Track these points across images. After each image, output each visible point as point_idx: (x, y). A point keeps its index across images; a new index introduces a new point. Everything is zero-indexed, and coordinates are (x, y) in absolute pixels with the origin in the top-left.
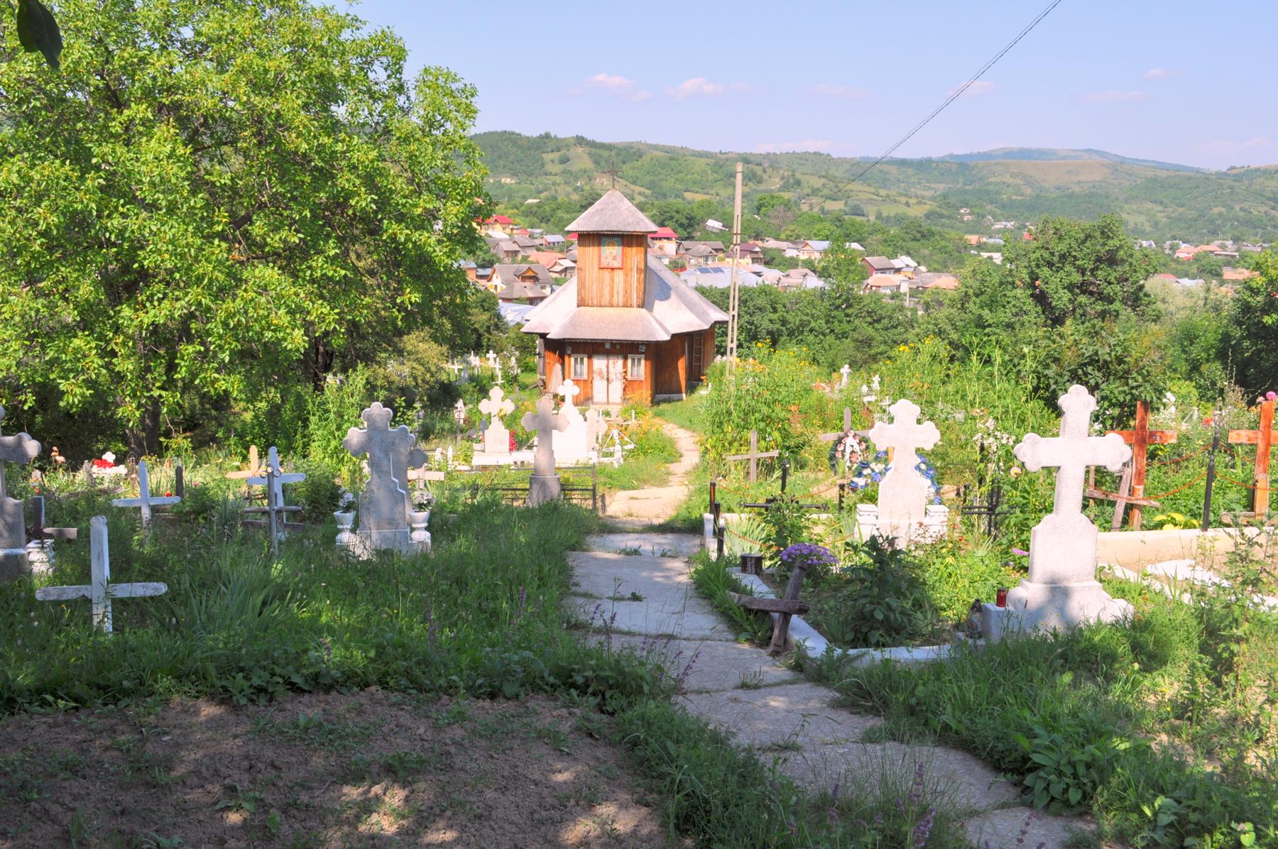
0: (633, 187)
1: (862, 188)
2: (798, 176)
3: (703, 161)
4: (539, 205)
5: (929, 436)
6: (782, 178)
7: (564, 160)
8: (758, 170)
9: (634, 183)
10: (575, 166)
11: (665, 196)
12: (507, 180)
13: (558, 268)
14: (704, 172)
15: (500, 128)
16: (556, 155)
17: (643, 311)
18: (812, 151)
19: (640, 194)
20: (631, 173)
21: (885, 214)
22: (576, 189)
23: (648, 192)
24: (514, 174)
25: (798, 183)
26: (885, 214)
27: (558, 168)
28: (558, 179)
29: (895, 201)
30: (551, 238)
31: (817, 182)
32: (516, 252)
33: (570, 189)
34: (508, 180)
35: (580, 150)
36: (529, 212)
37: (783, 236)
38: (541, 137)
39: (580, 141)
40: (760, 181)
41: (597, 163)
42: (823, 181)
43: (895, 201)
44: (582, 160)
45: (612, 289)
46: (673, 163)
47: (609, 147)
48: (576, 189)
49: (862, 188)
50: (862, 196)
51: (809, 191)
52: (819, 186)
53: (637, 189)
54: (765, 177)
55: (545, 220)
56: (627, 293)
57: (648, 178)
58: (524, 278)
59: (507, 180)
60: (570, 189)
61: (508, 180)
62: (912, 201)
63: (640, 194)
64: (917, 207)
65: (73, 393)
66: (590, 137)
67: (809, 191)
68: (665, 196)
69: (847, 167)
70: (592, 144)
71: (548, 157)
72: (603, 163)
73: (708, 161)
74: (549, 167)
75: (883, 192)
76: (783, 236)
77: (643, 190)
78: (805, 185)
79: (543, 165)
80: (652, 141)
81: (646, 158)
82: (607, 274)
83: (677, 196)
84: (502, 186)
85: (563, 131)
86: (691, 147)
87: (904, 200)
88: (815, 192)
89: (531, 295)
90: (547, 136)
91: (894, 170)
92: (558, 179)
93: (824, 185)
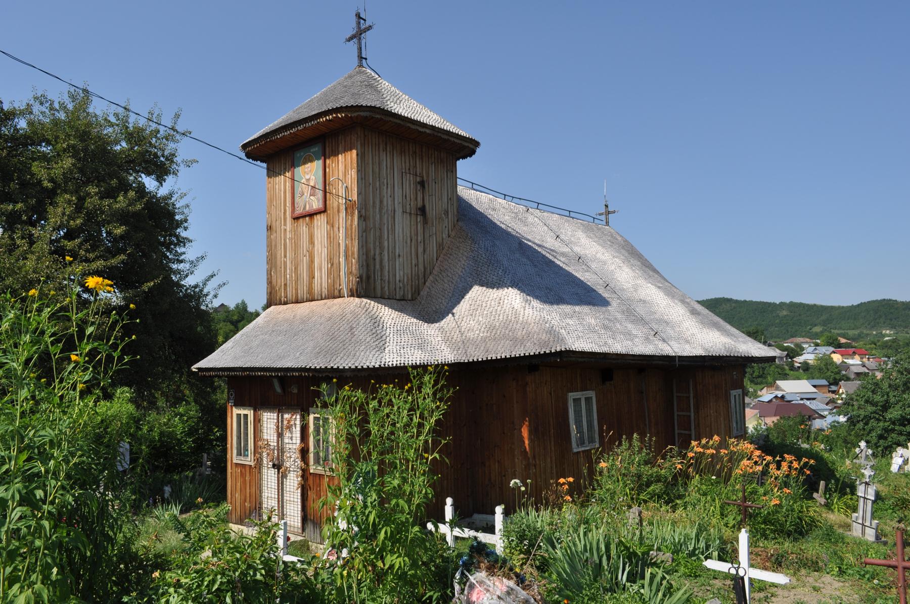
24: (892, 327)
45: (312, 261)
82: (303, 226)
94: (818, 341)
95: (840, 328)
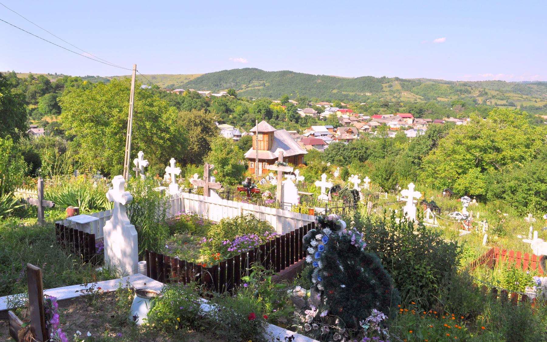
0: (417, 96)
1: (515, 95)
2: (486, 91)
3: (446, 85)
4: (365, 105)
5: (419, 195)
6: (480, 91)
7: (391, 86)
8: (469, 88)
9: (417, 94)
10: (394, 89)
11: (429, 99)
12: (368, 94)
13: (363, 129)
14: (446, 90)
15: (366, 75)
16: (387, 84)
17: (269, 152)
18: (497, 80)
19: (419, 98)
20: (416, 90)
21: (524, 106)
22: (394, 97)
23: (422, 98)
24: (371, 92)
25: (486, 93)
26: (524, 106)
27: (388, 89)
28: (387, 93)
29: (530, 100)
30: (365, 117)
31: (494, 93)
32: (350, 123)
33: (392, 97)
34: (368, 94)
35: (396, 82)
36: (361, 108)
37: (458, 117)
38: (382, 78)
39: (397, 79)
40: (470, 93)
41: (403, 87)
42: (498, 92)
43: (530, 100)
44: (397, 86)
46: (433, 87)
47: (409, 81)
48: (394, 97)
49: (515, 95)
50: (514, 98)
51: (491, 96)
52: (496, 94)
53: (418, 96)
54: (472, 91)
55: (366, 110)
56: (264, 146)
57: (423, 92)
58: (348, 132)
59: (368, 94)
60: (392, 97)
61: (368, 94)
62: (537, 100)
63: (419, 98)
64: (540, 103)
65: (173, 169)
66: (400, 78)
67: (491, 96)
68: (429, 99)
69: (513, 86)
70: (402, 80)
71: (384, 85)
72: (405, 87)
73: (448, 85)
74: (384, 89)
75: (524, 96)
76: (458, 117)
77: (420, 97)
78: (489, 94)
79: (382, 88)
80: (429, 77)
81: (423, 85)
82: (259, 142)
83: (434, 99)
84: (366, 96)
85: (390, 75)
86: (445, 80)
87: (534, 100)
88: (493, 97)
89: (348, 138)
90: (384, 77)
91: (535, 87)
92: (387, 93)
93: (498, 94)
94: (332, 104)
95: (346, 91)
